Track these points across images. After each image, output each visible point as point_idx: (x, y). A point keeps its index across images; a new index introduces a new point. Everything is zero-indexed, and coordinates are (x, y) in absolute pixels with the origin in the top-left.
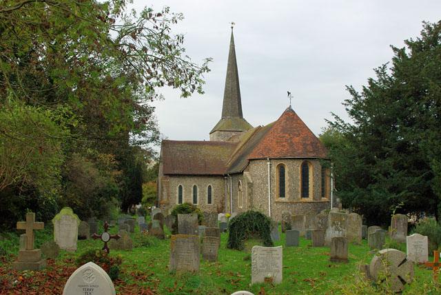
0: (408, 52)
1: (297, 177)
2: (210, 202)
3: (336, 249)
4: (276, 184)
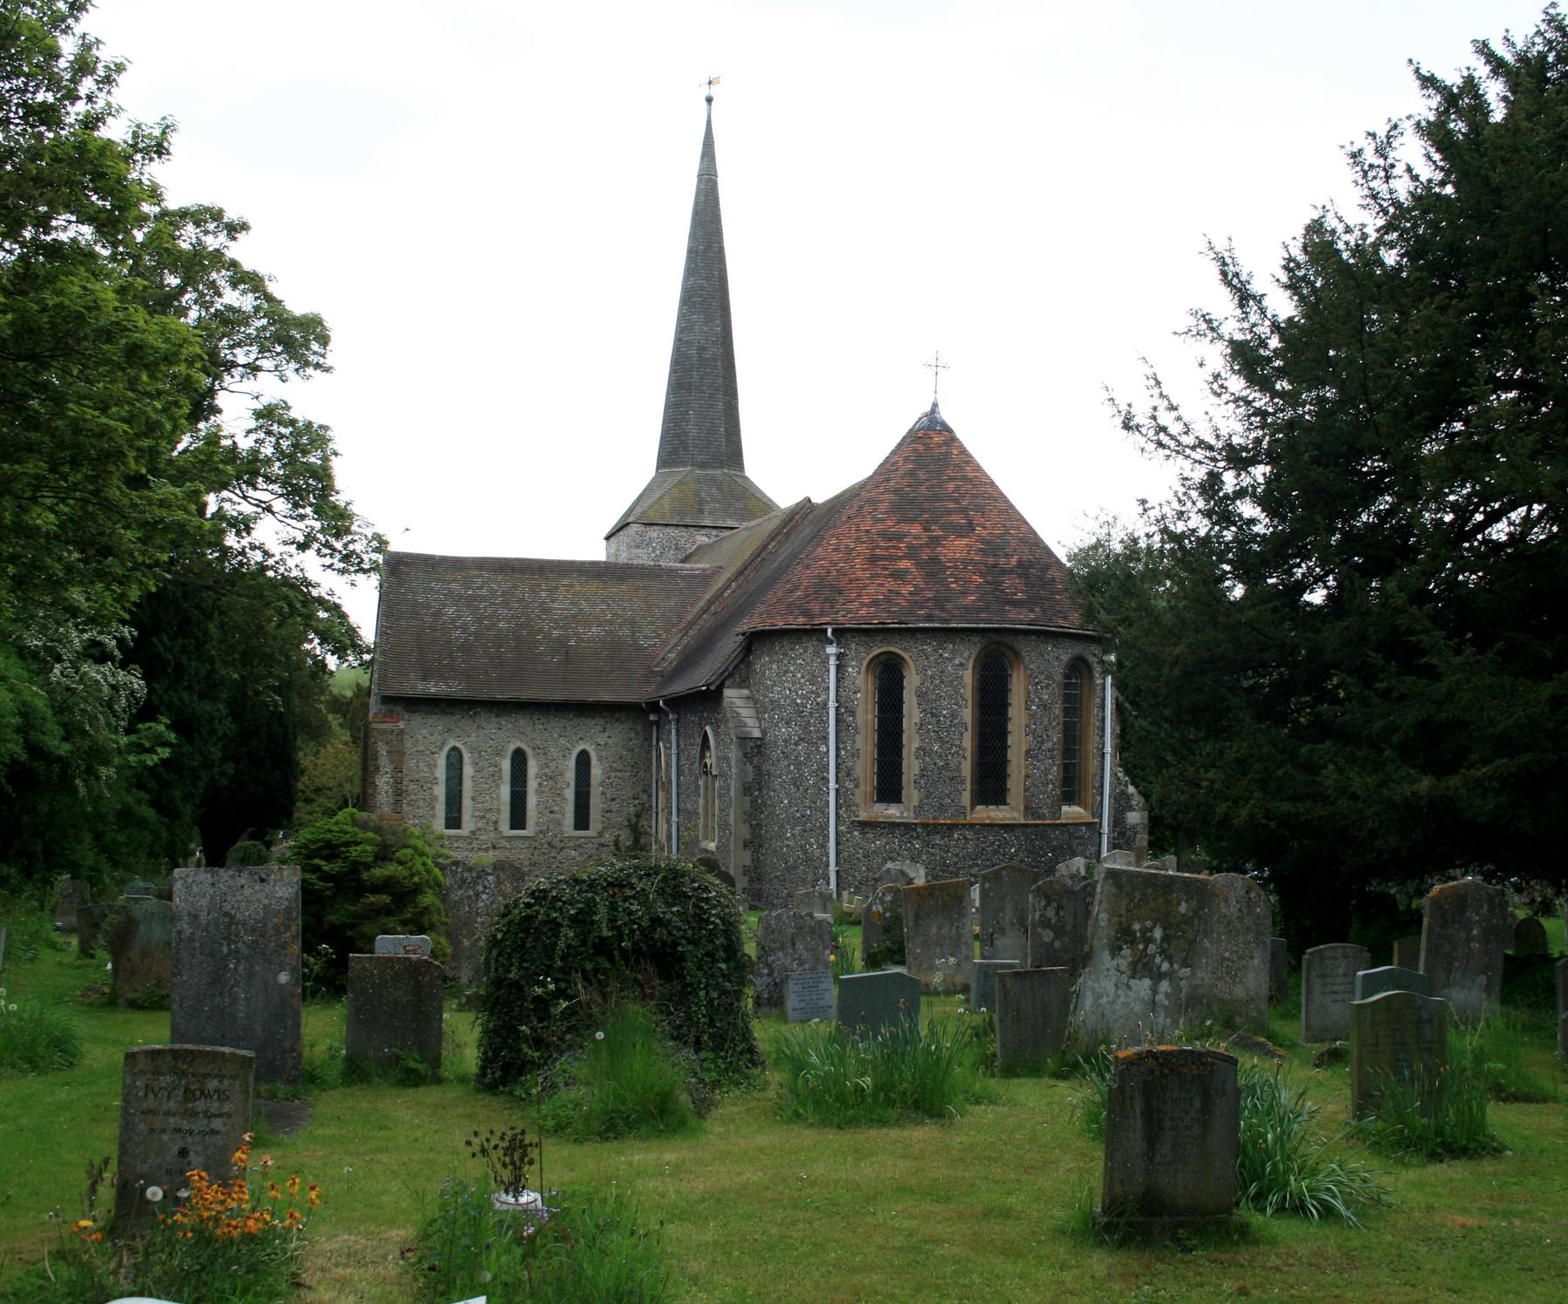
0: (1494, 91)
1: (954, 715)
2: (582, 821)
3: (1152, 1139)
4: (865, 742)
